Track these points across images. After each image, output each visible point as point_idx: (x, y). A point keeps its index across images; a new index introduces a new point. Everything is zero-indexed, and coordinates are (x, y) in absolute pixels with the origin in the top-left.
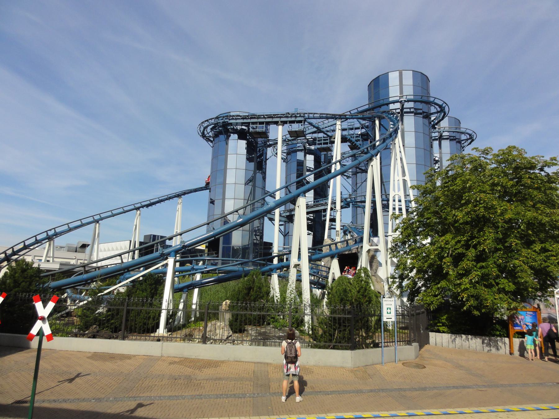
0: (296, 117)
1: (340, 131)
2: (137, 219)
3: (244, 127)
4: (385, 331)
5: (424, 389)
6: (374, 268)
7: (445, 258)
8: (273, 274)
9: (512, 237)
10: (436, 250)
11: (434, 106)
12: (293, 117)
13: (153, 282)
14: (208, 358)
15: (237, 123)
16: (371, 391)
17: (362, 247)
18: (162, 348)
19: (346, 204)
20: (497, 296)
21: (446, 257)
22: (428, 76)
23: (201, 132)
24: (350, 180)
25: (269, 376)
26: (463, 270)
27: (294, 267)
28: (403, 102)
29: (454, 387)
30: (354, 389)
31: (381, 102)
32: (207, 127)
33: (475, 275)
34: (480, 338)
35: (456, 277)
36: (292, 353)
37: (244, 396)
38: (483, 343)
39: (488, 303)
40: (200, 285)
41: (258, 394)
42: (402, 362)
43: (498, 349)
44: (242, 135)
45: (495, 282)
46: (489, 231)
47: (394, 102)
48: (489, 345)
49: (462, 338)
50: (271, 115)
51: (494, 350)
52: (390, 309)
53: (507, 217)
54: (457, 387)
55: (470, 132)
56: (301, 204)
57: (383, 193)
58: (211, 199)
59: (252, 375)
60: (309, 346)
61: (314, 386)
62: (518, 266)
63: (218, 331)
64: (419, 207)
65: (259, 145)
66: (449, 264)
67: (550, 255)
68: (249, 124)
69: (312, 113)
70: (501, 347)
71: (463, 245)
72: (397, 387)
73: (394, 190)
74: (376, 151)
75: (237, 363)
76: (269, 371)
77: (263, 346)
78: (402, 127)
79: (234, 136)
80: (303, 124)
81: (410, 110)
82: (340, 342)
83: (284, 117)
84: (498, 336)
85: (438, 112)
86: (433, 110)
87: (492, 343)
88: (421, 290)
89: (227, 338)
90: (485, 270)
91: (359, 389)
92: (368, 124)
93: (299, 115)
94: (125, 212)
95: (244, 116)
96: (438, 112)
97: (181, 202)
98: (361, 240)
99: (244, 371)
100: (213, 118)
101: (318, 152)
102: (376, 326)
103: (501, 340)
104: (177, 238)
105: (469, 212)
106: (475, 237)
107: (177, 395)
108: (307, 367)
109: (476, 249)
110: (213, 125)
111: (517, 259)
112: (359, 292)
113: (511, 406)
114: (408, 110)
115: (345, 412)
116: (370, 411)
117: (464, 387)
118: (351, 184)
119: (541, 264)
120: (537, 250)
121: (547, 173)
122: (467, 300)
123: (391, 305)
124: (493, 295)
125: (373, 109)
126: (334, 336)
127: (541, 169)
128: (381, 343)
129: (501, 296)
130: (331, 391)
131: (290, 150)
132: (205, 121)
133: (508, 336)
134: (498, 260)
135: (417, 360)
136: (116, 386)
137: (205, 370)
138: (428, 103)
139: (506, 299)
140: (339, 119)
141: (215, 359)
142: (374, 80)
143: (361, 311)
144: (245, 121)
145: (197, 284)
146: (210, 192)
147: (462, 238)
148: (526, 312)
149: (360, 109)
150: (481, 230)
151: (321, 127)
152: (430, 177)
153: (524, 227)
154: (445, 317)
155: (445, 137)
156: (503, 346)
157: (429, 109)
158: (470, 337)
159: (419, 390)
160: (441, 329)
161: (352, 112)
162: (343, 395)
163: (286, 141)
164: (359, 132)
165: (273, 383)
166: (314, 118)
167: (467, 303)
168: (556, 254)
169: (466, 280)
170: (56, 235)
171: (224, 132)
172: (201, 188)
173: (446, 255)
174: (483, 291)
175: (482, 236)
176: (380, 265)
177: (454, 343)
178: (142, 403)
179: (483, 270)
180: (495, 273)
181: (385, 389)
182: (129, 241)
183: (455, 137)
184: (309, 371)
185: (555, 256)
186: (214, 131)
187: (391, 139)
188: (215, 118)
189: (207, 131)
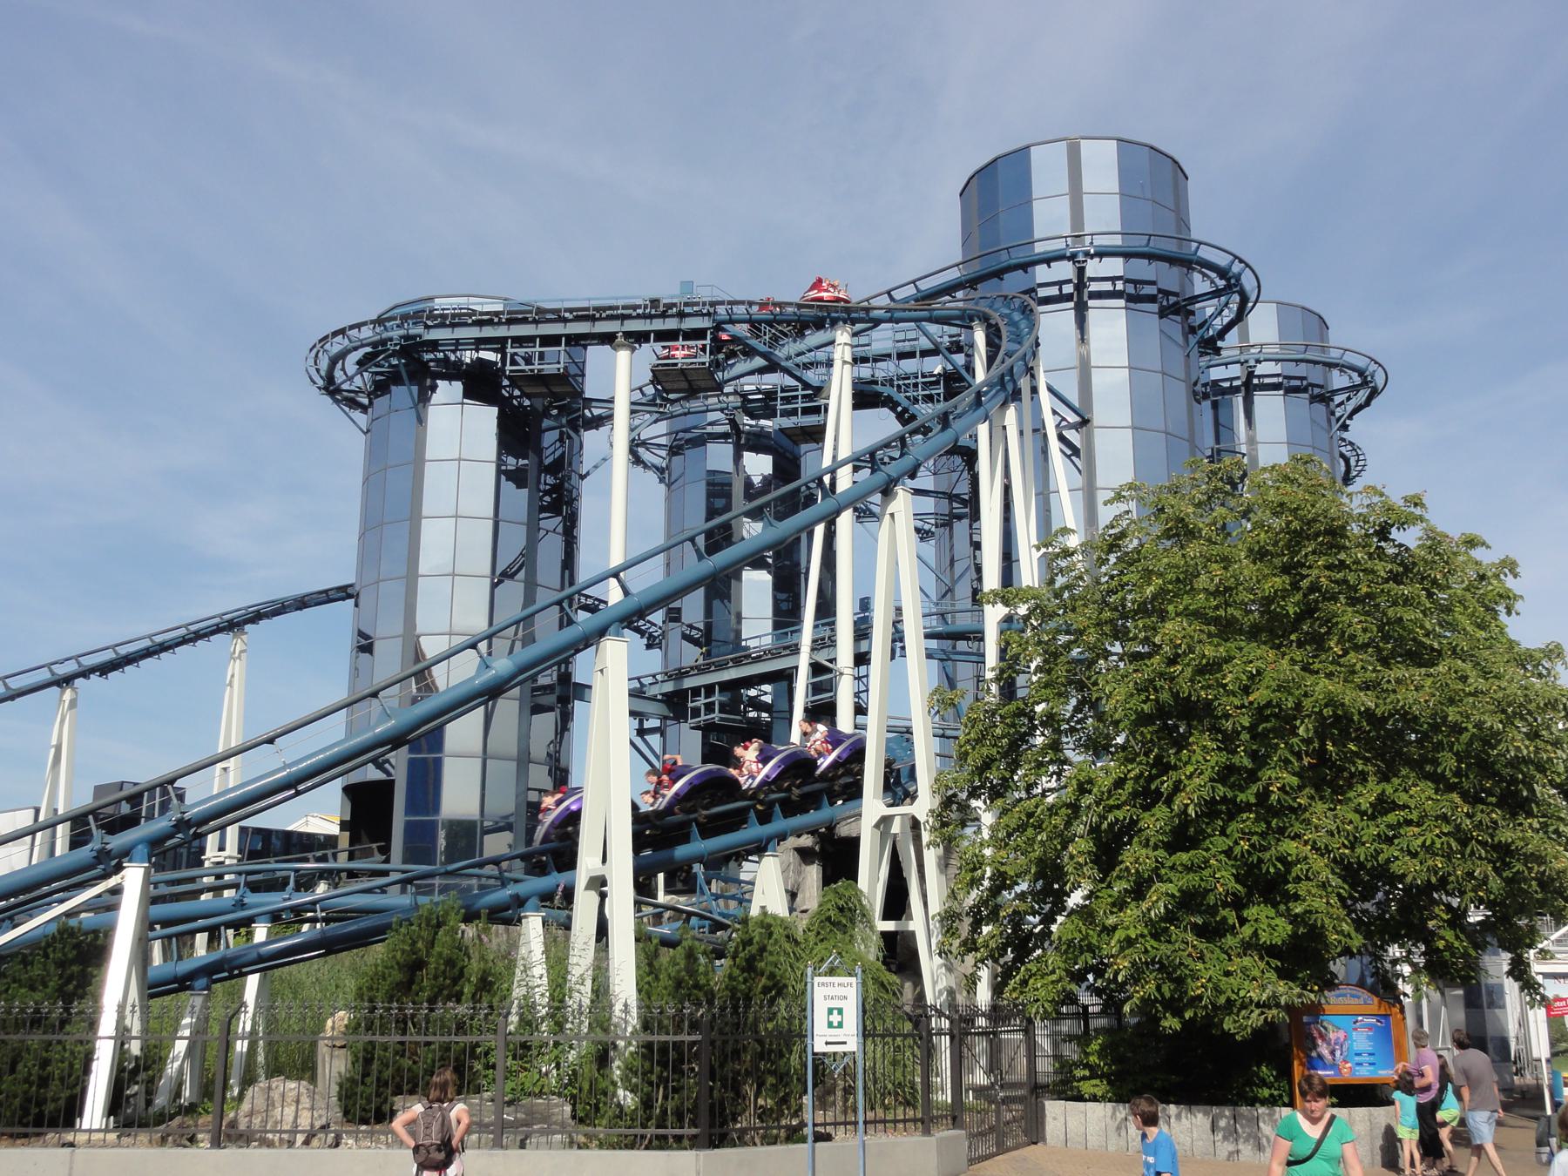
1: (848, 367)
8: (526, 917)
13: (70, 956)
15: (457, 340)
18: (71, 1168)
22: (1177, 158)
23: (323, 374)
27: (587, 888)
28: (1081, 258)
31: (1005, 259)
32: (342, 355)
33: (1157, 902)
34: (1206, 1114)
36: (430, 1135)
39: (1198, 988)
40: (266, 962)
43: (1260, 1148)
47: (1048, 260)
48: (1231, 1134)
50: (587, 309)
51: (1246, 1150)
52: (840, 1011)
53: (1260, 695)
55: (1360, 362)
56: (609, 664)
58: (361, 634)
66: (1081, 860)
69: (742, 303)
79: (448, 391)
83: (639, 316)
84: (1264, 1102)
85: (1216, 294)
86: (1200, 285)
87: (1242, 1126)
94: (12, 698)
96: (1216, 294)
97: (241, 652)
100: (364, 324)
101: (786, 442)
103: (1271, 1115)
105: (1151, 681)
110: (368, 349)
111: (1297, 837)
118: (933, 565)
119: (1378, 852)
120: (1365, 806)
123: (846, 998)
125: (971, 283)
129: (1247, 961)
131: (681, 435)
132: (335, 334)
138: (1187, 263)
142: (978, 172)
144: (488, 332)
146: (356, 605)
149: (924, 285)
151: (780, 355)
153: (1307, 730)
161: (898, 295)
163: (656, 405)
169: (1131, 913)
172: (326, 592)
174: (1184, 943)
177: (1123, 1133)
182: (32, 812)
183: (1304, 378)
188: (373, 322)
189: (343, 369)
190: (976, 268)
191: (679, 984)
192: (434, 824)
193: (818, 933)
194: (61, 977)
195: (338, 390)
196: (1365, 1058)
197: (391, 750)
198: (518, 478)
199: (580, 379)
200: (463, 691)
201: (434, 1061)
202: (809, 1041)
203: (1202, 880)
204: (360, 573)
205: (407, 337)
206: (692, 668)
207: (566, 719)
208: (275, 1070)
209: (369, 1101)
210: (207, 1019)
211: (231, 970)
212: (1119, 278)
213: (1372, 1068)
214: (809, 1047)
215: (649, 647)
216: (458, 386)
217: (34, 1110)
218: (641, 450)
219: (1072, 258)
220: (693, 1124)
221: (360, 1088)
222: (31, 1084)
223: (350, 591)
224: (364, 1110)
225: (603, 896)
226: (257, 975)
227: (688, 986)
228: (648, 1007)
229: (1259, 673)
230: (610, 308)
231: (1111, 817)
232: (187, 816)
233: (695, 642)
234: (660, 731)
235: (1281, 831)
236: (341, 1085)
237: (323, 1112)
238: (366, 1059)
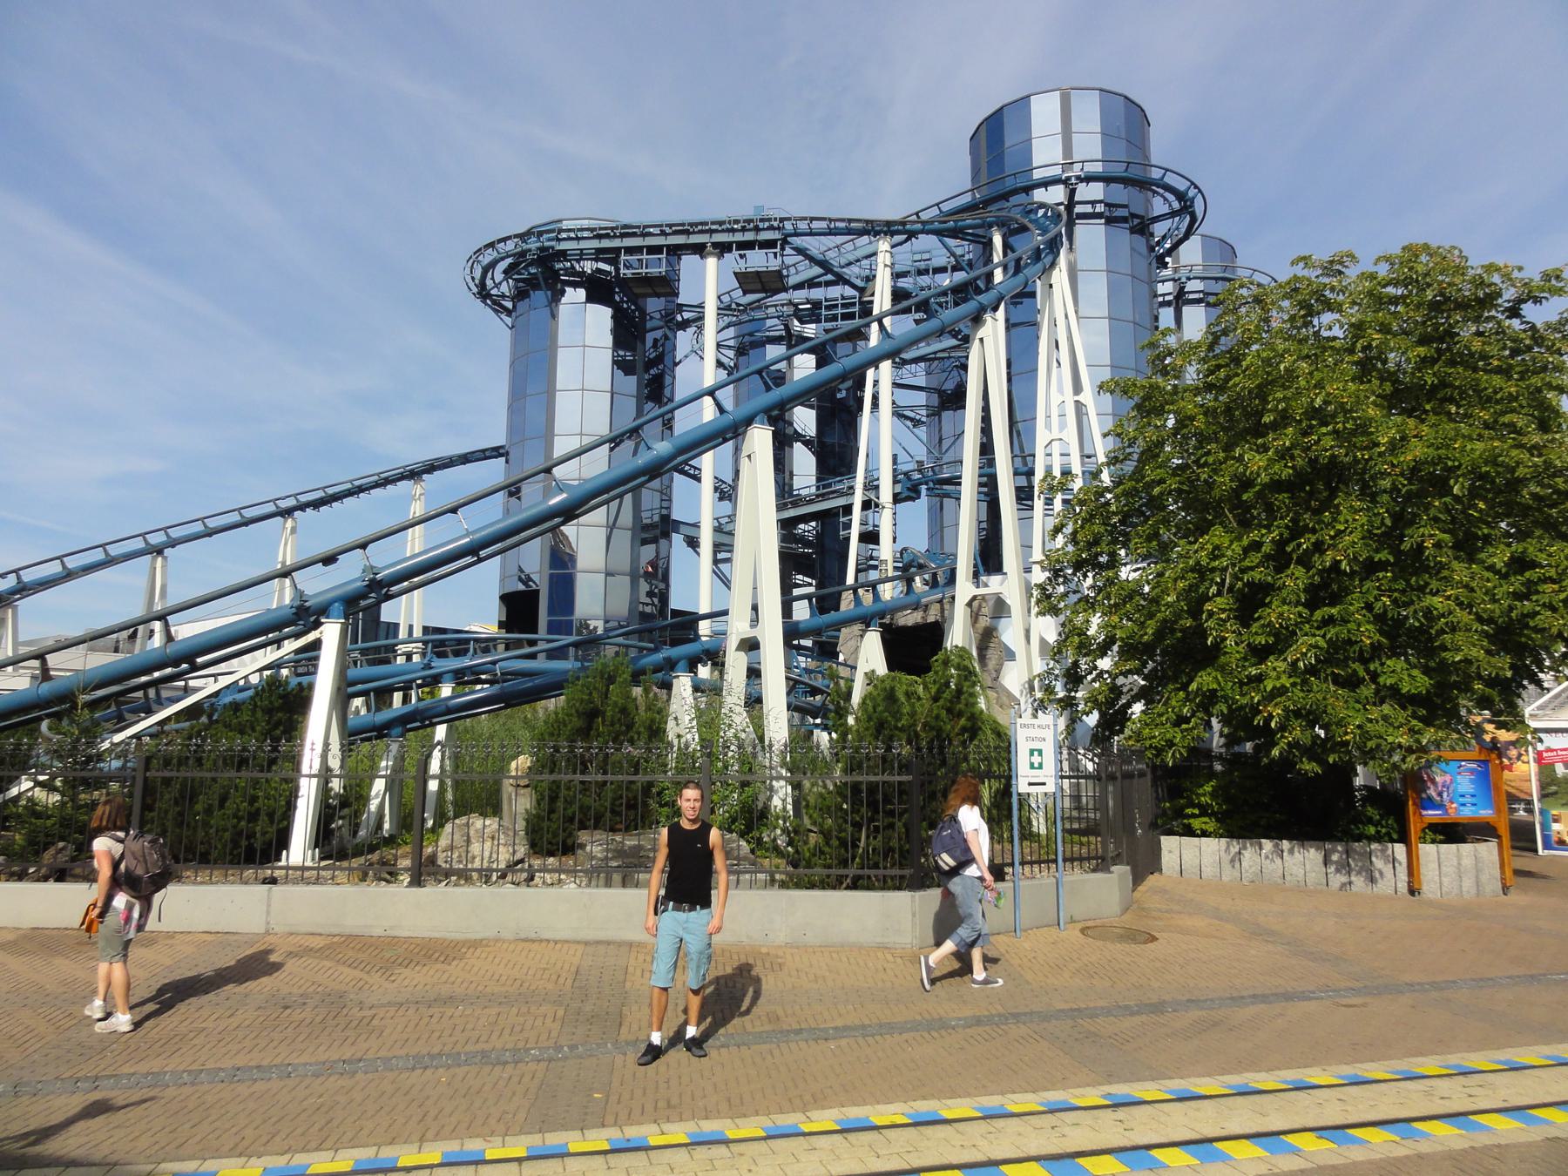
2: (286, 544)
4: (1023, 837)
5: (1158, 1008)
6: (991, 664)
7: (1209, 599)
9: (1423, 523)
10: (1183, 578)
11: (1162, 196)
12: (750, 230)
13: (276, 704)
14: (427, 934)
15: (581, 250)
16: (978, 1021)
17: (953, 598)
18: (269, 905)
19: (909, 489)
20: (1375, 713)
21: (1214, 596)
23: (477, 282)
24: (922, 431)
25: (628, 984)
26: (1269, 634)
29: (1254, 996)
30: (918, 1018)
31: (1010, 184)
32: (492, 265)
33: (1306, 647)
34: (1317, 849)
35: (1245, 659)
37: (518, 1056)
38: (1326, 862)
39: (1346, 733)
40: (450, 713)
41: (573, 1047)
42: (1080, 925)
43: (1372, 880)
44: (598, 290)
45: (1367, 671)
46: (1352, 506)
47: (1046, 183)
49: (1261, 849)
50: (683, 225)
51: (1359, 882)
52: (1040, 752)
54: (1256, 998)
56: (757, 450)
57: (1017, 451)
59: (569, 982)
60: (773, 881)
61: (780, 1012)
62: (1443, 616)
63: (475, 848)
64: (1128, 450)
65: (649, 325)
66: (1223, 616)
67: (1539, 578)
68: (618, 256)
69: (805, 219)
70: (1381, 873)
71: (1267, 557)
72: (1066, 1006)
73: (1048, 426)
74: (992, 295)
75: (523, 944)
76: (631, 969)
77: (624, 885)
78: (1071, 257)
79: (575, 295)
80: (778, 250)
81: (1094, 207)
82: (876, 866)
83: (723, 231)
84: (1371, 839)
85: (1173, 214)
86: (1159, 206)
87: (1354, 860)
88: (1132, 713)
90: (1337, 629)
91: (936, 1017)
92: (971, 255)
93: (767, 224)
95: (601, 229)
96: (1173, 214)
98: (951, 580)
99: (545, 969)
100: (509, 238)
102: (994, 812)
103: (1383, 851)
104: (412, 599)
105: (1289, 449)
106: (1306, 529)
107: (265, 1063)
108: (764, 950)
110: (510, 260)
112: (936, 699)
113: (1465, 1055)
114: (1088, 209)
115: (878, 1103)
116: (969, 1095)
117: (1288, 997)
118: (925, 441)
119: (1511, 608)
120: (1500, 565)
121: (1528, 323)
122: (1283, 728)
125: (987, 202)
126: (855, 846)
127: (1514, 312)
128: (1012, 864)
130: (836, 1028)
133: (1404, 838)
134: (1377, 599)
135: (1127, 917)
136: (48, 1039)
137: (407, 972)
138: (1144, 185)
139: (1403, 721)
140: (886, 234)
141: (449, 936)
142: (986, 119)
143: (944, 763)
144: (606, 243)
145: (434, 711)
146: (507, 462)
147: (1263, 535)
148: (1457, 764)
149: (946, 207)
150: (1327, 504)
152: (1160, 362)
154: (1208, 788)
155: (1192, 296)
156: (1388, 870)
158: (1286, 844)
159: (1138, 1013)
160: (1197, 824)
161: (924, 216)
162: (878, 1038)
164: (945, 281)
165: (635, 1008)
166: (811, 234)
167: (1282, 737)
168: (1558, 573)
171: (545, 280)
172: (483, 451)
173: (1214, 589)
175: (1327, 525)
176: (1011, 655)
177: (1237, 865)
178: (108, 1100)
179: (1332, 632)
180: (1369, 637)
181: (1025, 1014)
184: (768, 965)
185: (1553, 581)
187: (1039, 266)
189: (493, 279)
190: (986, 192)
194: (268, 722)
195: (489, 296)
196: (1468, 799)
197: (563, 523)
205: (542, 249)
208: (463, 808)
209: (555, 835)
210: (403, 759)
211: (422, 721)
212: (1100, 202)
217: (244, 843)
219: (1066, 182)
221: (546, 824)
222: (240, 819)
223: (502, 451)
224: (550, 843)
230: (702, 224)
235: (1421, 589)
236: (527, 821)
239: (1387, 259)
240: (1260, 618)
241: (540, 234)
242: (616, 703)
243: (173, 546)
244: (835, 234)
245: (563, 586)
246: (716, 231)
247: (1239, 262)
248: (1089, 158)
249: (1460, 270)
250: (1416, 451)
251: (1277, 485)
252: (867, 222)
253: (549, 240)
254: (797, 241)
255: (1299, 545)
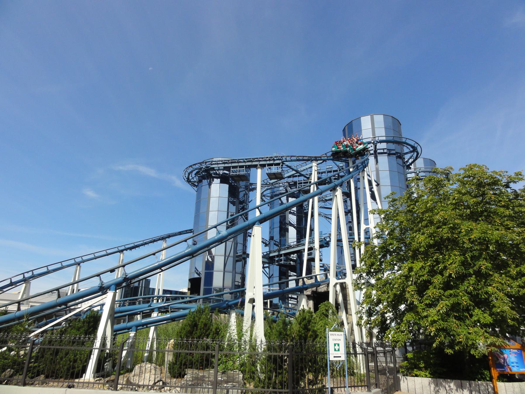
0: (274, 160)
3: (225, 172)
15: (219, 167)
20: (471, 330)
21: (410, 285)
23: (187, 177)
32: (192, 172)
33: (443, 306)
39: (460, 338)
44: (224, 179)
50: (250, 159)
52: (338, 345)
79: (217, 181)
83: (263, 161)
85: (411, 152)
86: (406, 150)
89: (155, 383)
95: (225, 161)
109: (442, 275)
110: (197, 171)
114: (382, 151)
119: (519, 291)
121: (513, 190)
124: (467, 329)
127: (507, 186)
138: (400, 143)
144: (226, 165)
148: (509, 350)
151: (300, 170)
153: (493, 248)
157: (402, 149)
163: (267, 185)
166: (291, 161)
170: (34, 277)
172: (186, 231)
174: (453, 323)
180: (466, 302)
186: (199, 176)
189: (191, 176)
191: (280, 333)
192: (212, 288)
193: (320, 318)
198: (233, 203)
199: (248, 177)
200: (212, 240)
201: (198, 357)
202: (328, 356)
203: (458, 300)
204: (194, 226)
205: (207, 167)
206: (276, 250)
207: (245, 263)
213: (517, 368)
214: (328, 358)
215: (265, 246)
216: (219, 180)
217: (71, 371)
218: (263, 198)
220: (287, 389)
222: (71, 362)
225: (254, 307)
226: (154, 327)
227: (283, 335)
228: (269, 342)
229: (471, 230)
230: (256, 158)
231: (421, 279)
232: (127, 277)
233: (277, 245)
234: (269, 267)
237: (159, 376)
238: (177, 356)
239: (463, 169)
240: (426, 294)
241: (206, 163)
242: (202, 322)
243: (83, 262)
244: (299, 161)
245: (209, 277)
246: (261, 161)
247: (437, 166)
248: (381, 136)
249: (484, 173)
250: (475, 235)
251: (430, 246)
252: (309, 157)
253: (209, 164)
254: (287, 163)
255: (439, 267)
